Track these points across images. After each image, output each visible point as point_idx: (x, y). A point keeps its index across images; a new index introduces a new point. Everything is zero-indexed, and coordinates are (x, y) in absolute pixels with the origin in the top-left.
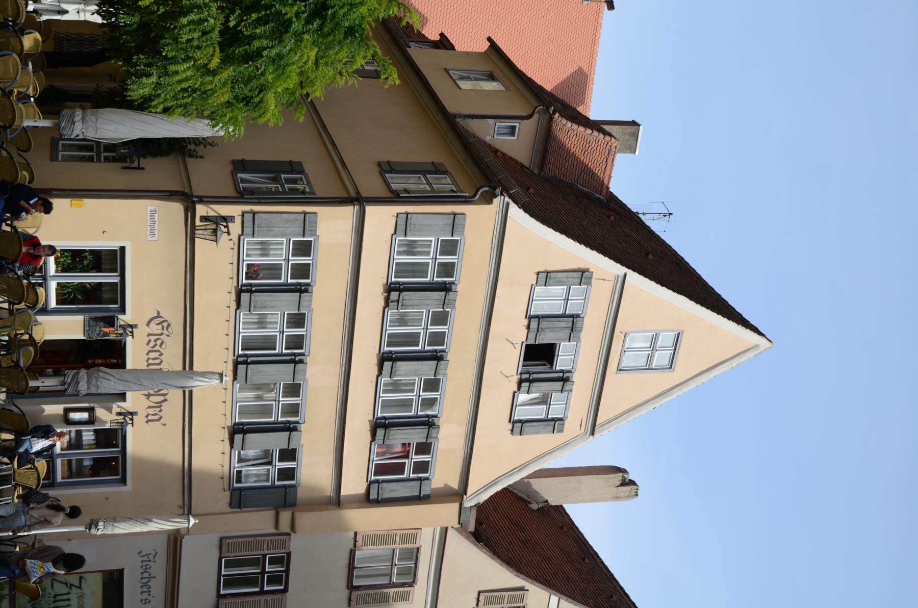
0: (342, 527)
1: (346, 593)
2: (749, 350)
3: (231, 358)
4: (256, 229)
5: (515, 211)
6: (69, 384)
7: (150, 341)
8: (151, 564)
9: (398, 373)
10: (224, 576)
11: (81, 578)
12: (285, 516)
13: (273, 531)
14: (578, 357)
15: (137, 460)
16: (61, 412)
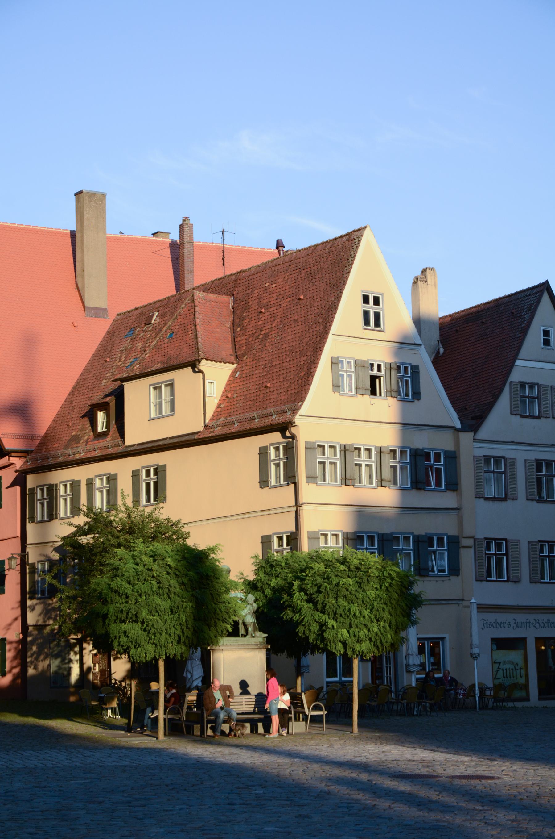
8: (488, 622)
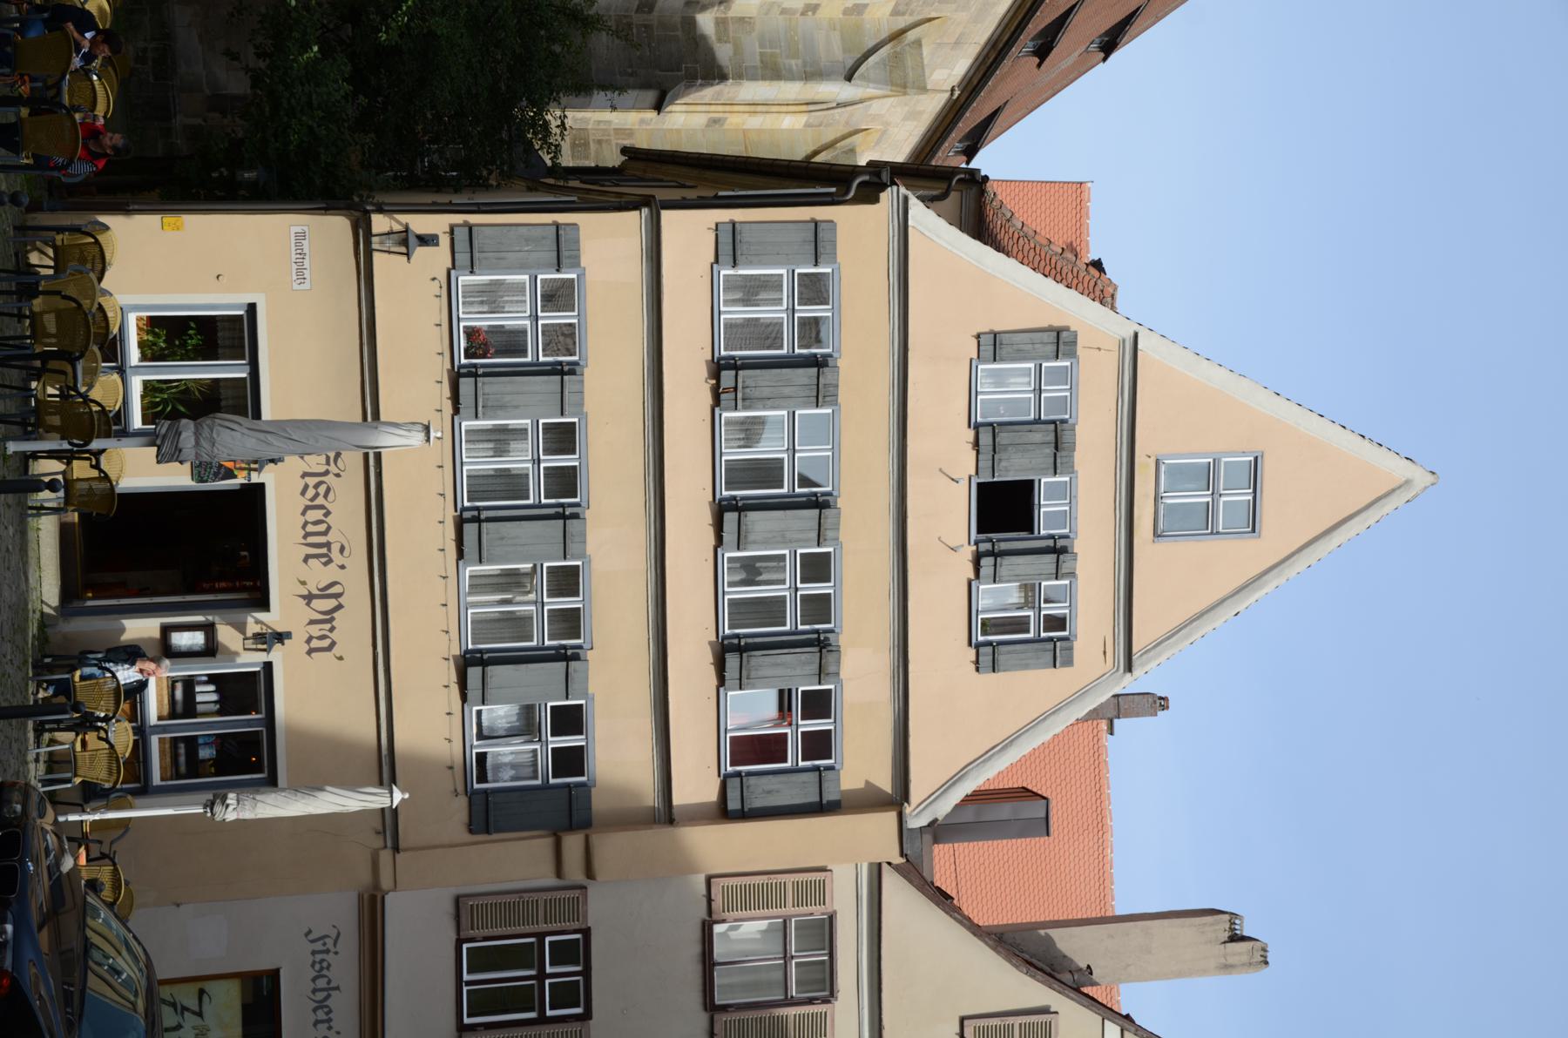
0: (682, 865)
1: (702, 1018)
2: (1393, 490)
3: (450, 514)
4: (476, 255)
5: (917, 209)
6: (164, 437)
7: (306, 487)
8: (330, 957)
9: (751, 537)
10: (469, 983)
11: (202, 992)
12: (573, 844)
13: (552, 881)
14: (1080, 503)
15: (292, 732)
16: (157, 634)
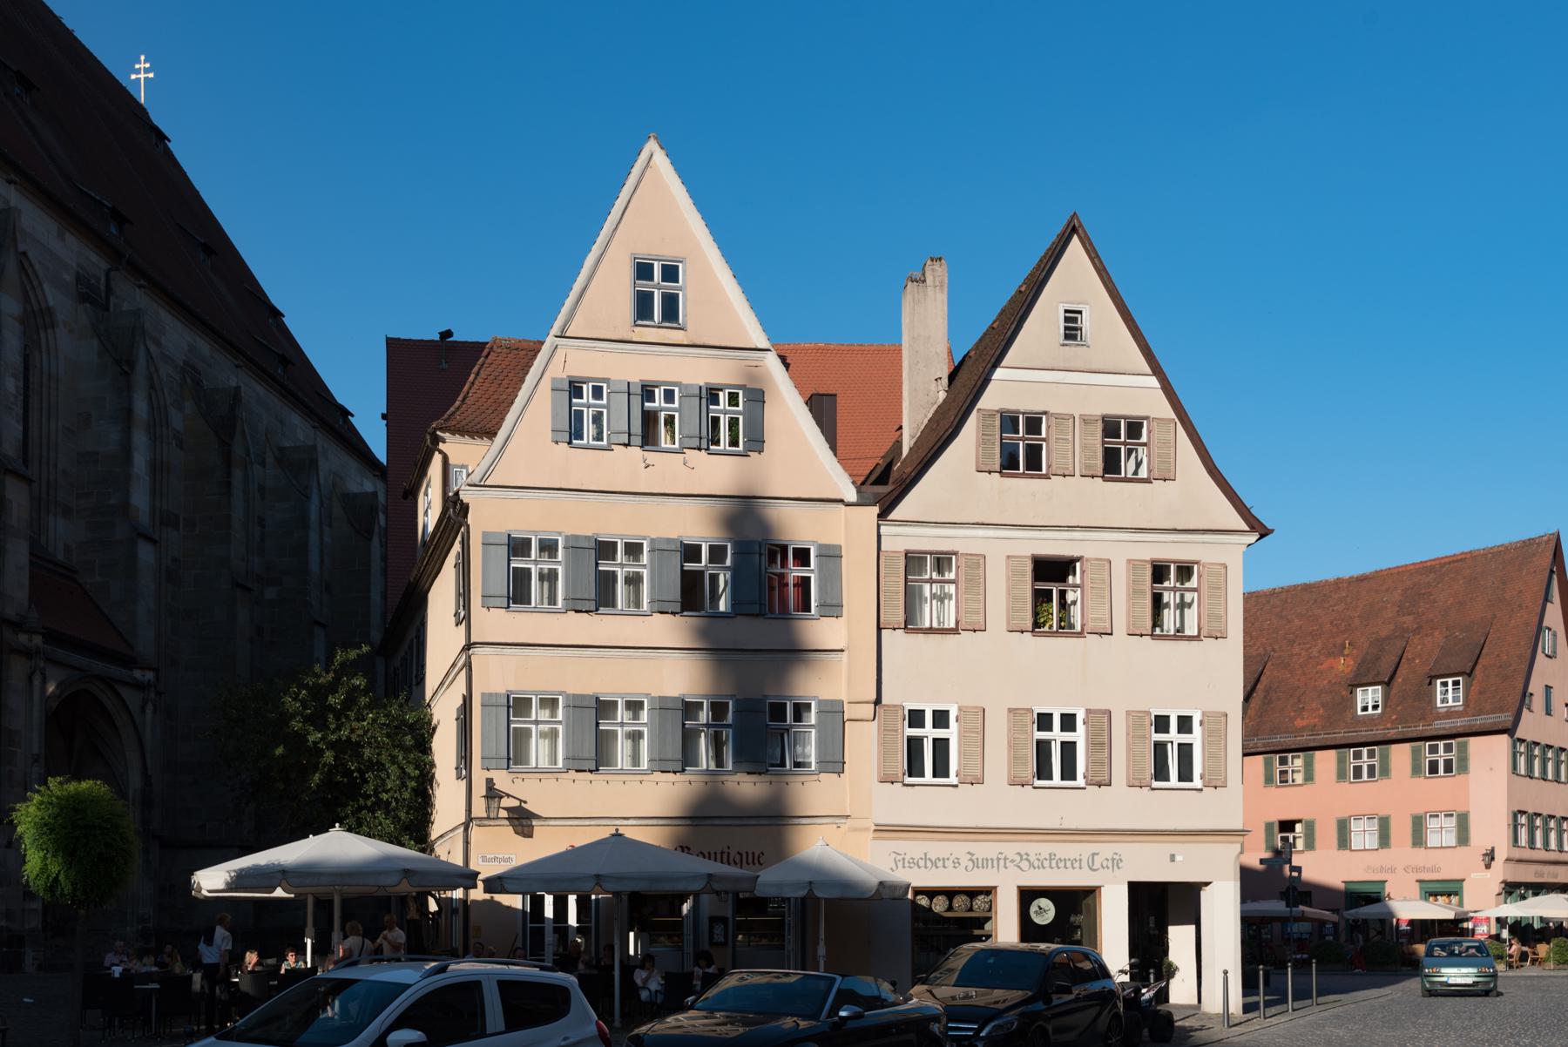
8: (907, 858)
